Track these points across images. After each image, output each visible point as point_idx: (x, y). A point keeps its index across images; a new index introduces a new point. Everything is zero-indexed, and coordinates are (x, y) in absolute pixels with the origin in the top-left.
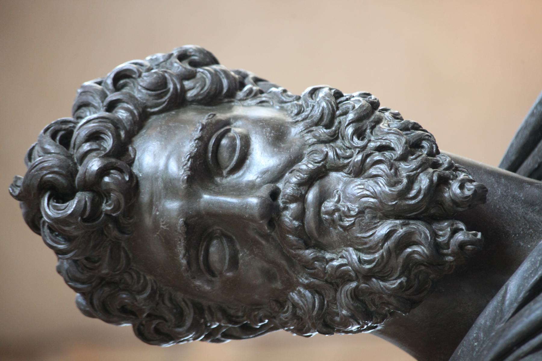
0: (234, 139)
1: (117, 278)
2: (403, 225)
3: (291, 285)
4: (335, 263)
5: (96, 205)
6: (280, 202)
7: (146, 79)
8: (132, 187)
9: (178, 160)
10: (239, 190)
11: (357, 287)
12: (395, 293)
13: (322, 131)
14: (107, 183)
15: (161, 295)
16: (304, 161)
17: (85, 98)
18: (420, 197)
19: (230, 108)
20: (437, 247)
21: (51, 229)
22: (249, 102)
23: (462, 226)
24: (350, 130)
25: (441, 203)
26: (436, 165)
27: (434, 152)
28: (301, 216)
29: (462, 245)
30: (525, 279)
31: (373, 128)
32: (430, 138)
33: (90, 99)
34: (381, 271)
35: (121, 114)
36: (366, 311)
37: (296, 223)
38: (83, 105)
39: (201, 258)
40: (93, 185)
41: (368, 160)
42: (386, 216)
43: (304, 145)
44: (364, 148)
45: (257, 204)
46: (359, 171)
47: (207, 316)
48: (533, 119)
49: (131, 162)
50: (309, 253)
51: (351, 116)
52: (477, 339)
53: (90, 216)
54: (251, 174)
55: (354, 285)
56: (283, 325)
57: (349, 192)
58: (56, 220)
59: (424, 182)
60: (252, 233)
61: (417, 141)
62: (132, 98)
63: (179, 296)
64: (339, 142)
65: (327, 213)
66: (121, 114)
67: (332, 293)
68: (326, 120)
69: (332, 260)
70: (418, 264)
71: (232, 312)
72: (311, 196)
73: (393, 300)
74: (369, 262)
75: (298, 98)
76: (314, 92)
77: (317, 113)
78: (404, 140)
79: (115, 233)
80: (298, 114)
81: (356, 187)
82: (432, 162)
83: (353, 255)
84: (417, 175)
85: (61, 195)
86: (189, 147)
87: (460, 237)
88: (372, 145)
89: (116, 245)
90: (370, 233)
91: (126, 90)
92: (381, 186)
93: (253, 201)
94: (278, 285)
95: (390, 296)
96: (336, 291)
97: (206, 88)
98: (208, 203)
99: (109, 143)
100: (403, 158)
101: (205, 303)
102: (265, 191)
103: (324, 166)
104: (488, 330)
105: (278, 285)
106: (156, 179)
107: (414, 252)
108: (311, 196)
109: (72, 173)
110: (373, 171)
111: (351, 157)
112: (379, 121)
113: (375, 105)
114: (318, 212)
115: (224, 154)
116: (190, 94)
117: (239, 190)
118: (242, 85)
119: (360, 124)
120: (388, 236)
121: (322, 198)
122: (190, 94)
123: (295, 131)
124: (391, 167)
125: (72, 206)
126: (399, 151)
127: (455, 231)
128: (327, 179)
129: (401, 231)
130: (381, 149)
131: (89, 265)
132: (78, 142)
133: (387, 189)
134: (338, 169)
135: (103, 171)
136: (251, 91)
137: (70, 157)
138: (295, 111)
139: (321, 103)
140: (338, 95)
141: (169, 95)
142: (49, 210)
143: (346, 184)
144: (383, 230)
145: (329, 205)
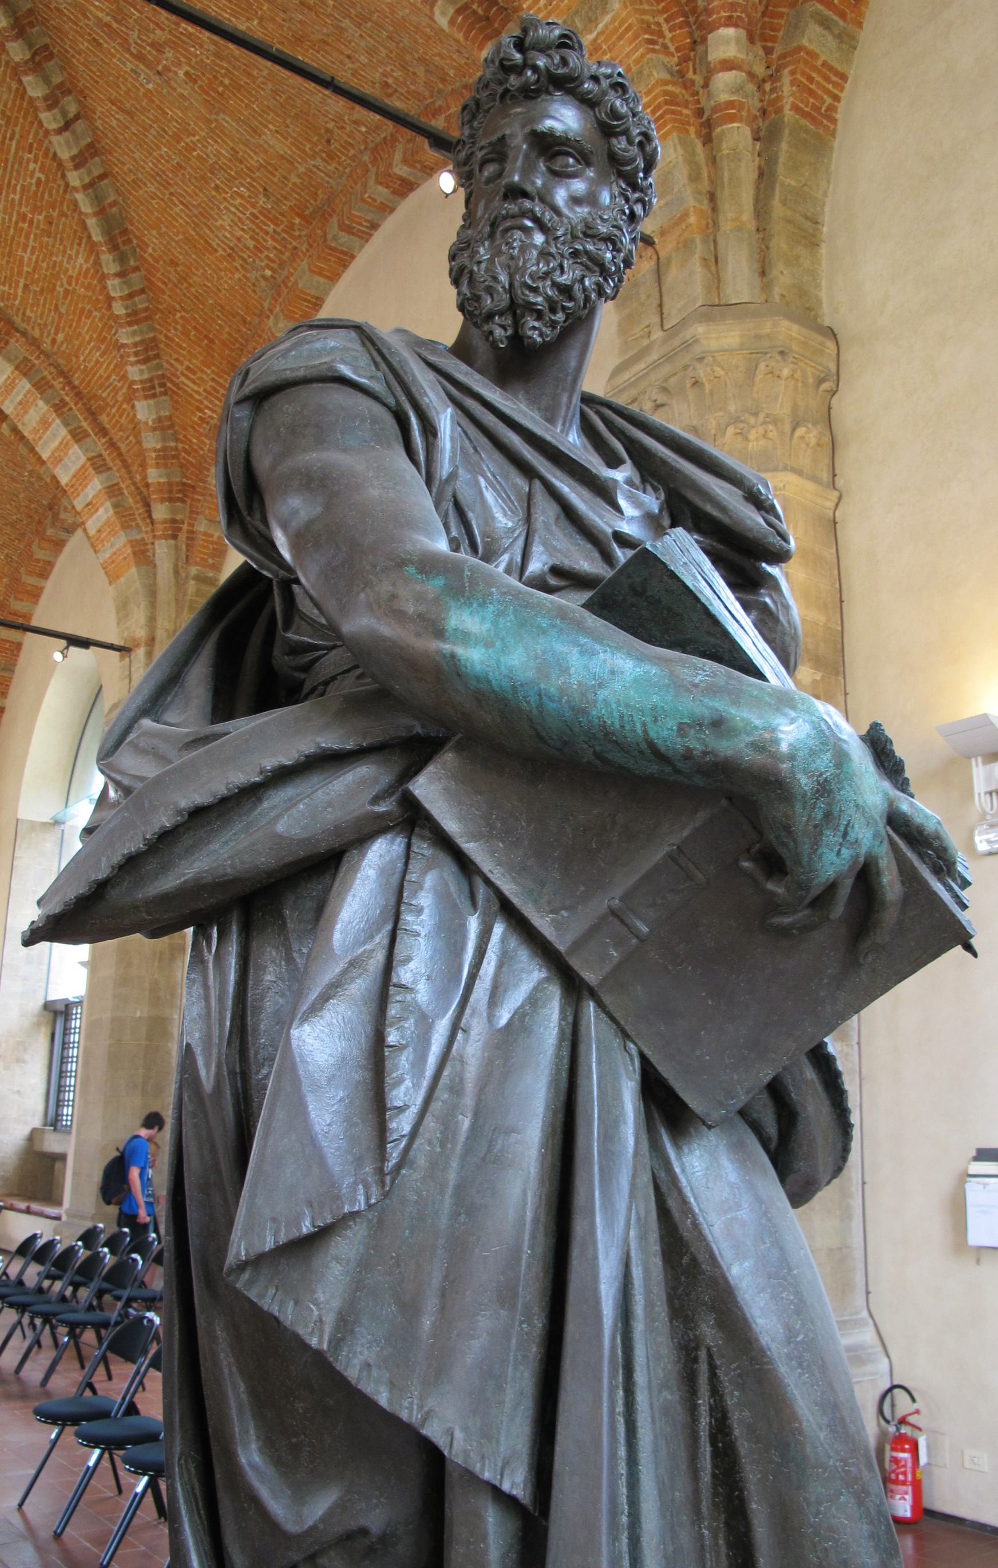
23: (510, 332)
68: (589, 232)
100: (555, 284)
127: (504, 327)
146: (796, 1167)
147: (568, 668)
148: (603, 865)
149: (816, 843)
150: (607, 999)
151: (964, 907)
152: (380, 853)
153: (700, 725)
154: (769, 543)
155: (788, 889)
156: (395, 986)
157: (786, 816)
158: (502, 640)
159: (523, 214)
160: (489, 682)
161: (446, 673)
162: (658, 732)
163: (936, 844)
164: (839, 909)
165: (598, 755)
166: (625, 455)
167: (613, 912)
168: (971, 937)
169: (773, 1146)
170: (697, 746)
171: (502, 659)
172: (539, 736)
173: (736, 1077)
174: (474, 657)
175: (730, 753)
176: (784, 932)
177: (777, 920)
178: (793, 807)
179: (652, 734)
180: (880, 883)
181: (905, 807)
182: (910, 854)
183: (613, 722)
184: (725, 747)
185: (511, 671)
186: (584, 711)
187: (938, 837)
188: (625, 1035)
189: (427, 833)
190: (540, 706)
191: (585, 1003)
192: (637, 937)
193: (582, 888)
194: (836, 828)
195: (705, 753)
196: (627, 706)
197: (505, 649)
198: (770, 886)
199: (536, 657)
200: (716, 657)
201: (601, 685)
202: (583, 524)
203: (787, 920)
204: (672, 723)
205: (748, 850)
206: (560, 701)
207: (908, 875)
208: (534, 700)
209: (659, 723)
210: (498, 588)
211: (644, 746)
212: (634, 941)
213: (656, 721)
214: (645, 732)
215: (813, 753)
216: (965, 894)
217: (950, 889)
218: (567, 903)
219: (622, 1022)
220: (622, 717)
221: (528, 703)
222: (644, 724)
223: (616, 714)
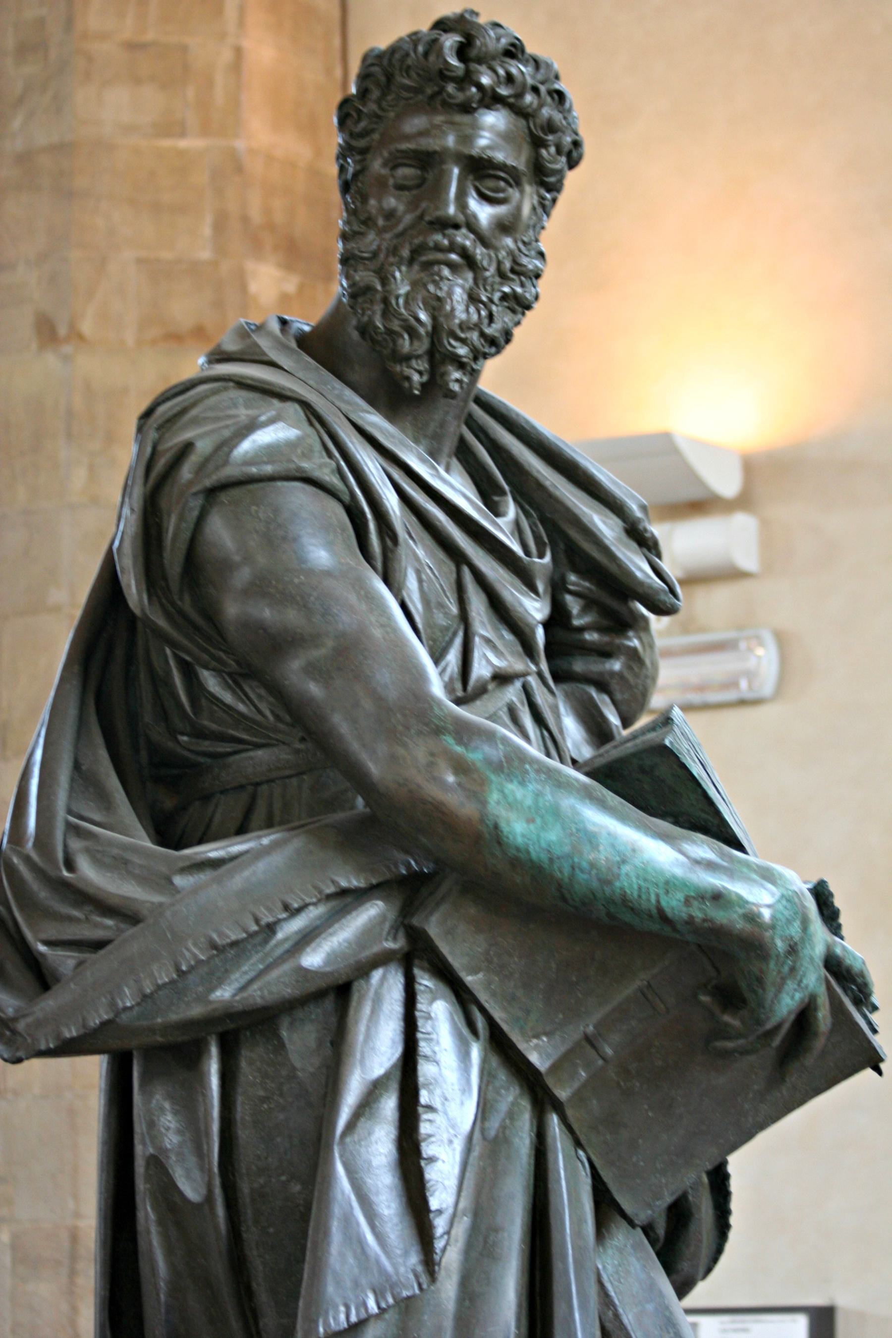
0: (503, 191)
1: (393, 88)
2: (427, 333)
3: (381, 231)
4: (398, 274)
5: (453, 79)
6: (450, 231)
7: (557, 117)
8: (467, 109)
9: (489, 147)
10: (461, 196)
11: (376, 290)
12: (371, 322)
13: (508, 265)
14: (470, 89)
15: (376, 123)
16: (484, 250)
17: (543, 66)
18: (449, 348)
19: (530, 184)
20: (407, 359)
21: (435, 41)
22: (536, 198)
23: (425, 378)
24: (506, 289)
25: (443, 363)
26: (475, 359)
27: (486, 356)
28: (438, 248)
29: (408, 379)
30: (380, 429)
31: (509, 308)
32: (498, 352)
33: (542, 71)
34: (388, 311)
35: (529, 98)
36: (358, 293)
37: (431, 244)
38: (537, 63)
39: (372, 526)
40: (468, 79)
41: (481, 306)
42: (434, 318)
43: (496, 249)
44: (491, 300)
45: (448, 214)
46: (473, 298)
47: (358, 157)
48: (514, 416)
49: (488, 107)
50: (406, 253)
51: (519, 290)
52: (334, 388)
53: (444, 74)
54: (474, 204)
55: (379, 288)
56: (347, 222)
57: (457, 291)
58: (441, 48)
59: (462, 351)
60: (424, 205)
61: (497, 344)
62: (541, 105)
63: (376, 136)
64: (497, 279)
65: (440, 270)
66: (529, 98)
67: (372, 267)
68: (517, 268)
69: (400, 271)
70: (394, 342)
71: (361, 178)
72: (454, 257)
73: (366, 319)
74: (397, 304)
75: (537, 241)
76: (541, 255)
77: (524, 261)
78: (497, 334)
79: (429, 91)
80: (524, 243)
81: (459, 294)
82: (478, 355)
83: (404, 289)
84: (467, 345)
85: (462, 52)
86: (500, 156)
87: (416, 377)
88: (494, 308)
89: (417, 91)
90: (421, 305)
91: (549, 99)
92: (461, 314)
93: (452, 210)
94: (381, 222)
95: (370, 317)
96: (374, 272)
97: (548, 165)
98: (451, 172)
99: (503, 91)
100: (482, 334)
101: (369, 156)
102: (461, 218)
103: (478, 267)
104: (340, 397)
105: (381, 222)
106: (473, 129)
107: (404, 339)
108: (454, 257)
109: (480, 61)
110: (472, 309)
111: (486, 290)
112: (514, 311)
113: (528, 307)
114: (439, 262)
115: (491, 183)
116: (544, 152)
117: (461, 196)
118: (549, 191)
119: (511, 298)
120: (418, 320)
121: (452, 266)
122: (544, 152)
123: (509, 242)
124: (476, 325)
125: (454, 61)
126: (488, 331)
127: (420, 373)
128: (466, 269)
129: (422, 331)
130: (491, 317)
131: (404, 67)
132: (507, 66)
133: (457, 321)
134: (475, 280)
135: (480, 87)
136: (543, 198)
137: (494, 58)
138: (525, 239)
139: (530, 263)
140: (538, 276)
141: (542, 135)
142: (450, 41)
143: (463, 287)
144: (423, 316)
145: (446, 272)
146: (679, 1267)
147: (598, 845)
148: (580, 995)
149: (780, 989)
150: (569, 1112)
151: (875, 1031)
152: (388, 986)
153: (703, 898)
154: (659, 601)
155: (743, 1022)
156: (423, 1106)
157: (761, 971)
158: (542, 817)
159: (452, 248)
160: (528, 852)
161: (487, 837)
162: (668, 902)
163: (859, 980)
164: (777, 1041)
165: (610, 915)
166: (507, 488)
167: (587, 1039)
168: (882, 1060)
169: (659, 1245)
170: (698, 915)
171: (542, 835)
172: (563, 899)
173: (663, 1181)
174: (517, 829)
175: (725, 921)
176: (725, 1054)
177: (719, 1044)
178: (768, 964)
179: (664, 903)
180: (816, 1017)
181: (838, 951)
182: (839, 990)
183: (632, 892)
184: (720, 916)
185: (549, 846)
186: (609, 883)
187: (862, 975)
188: (578, 1144)
189: (426, 965)
190: (572, 876)
191: (549, 1116)
192: (603, 1059)
193: (561, 1016)
194: (795, 978)
195: (704, 920)
196: (645, 880)
197: (544, 827)
198: (727, 1018)
199: (572, 834)
200: (705, 830)
201: (624, 862)
202: (511, 617)
203: (730, 1045)
204: (680, 896)
205: (705, 986)
206: (590, 873)
207: (837, 1008)
208: (567, 871)
209: (670, 895)
210: (530, 764)
211: (654, 911)
212: (600, 1062)
213: (667, 892)
214: (658, 901)
215: (789, 922)
216: (874, 1017)
217: (865, 1017)
218: (548, 1029)
219: (578, 1133)
220: (640, 888)
221: (561, 872)
222: (657, 895)
223: (635, 886)
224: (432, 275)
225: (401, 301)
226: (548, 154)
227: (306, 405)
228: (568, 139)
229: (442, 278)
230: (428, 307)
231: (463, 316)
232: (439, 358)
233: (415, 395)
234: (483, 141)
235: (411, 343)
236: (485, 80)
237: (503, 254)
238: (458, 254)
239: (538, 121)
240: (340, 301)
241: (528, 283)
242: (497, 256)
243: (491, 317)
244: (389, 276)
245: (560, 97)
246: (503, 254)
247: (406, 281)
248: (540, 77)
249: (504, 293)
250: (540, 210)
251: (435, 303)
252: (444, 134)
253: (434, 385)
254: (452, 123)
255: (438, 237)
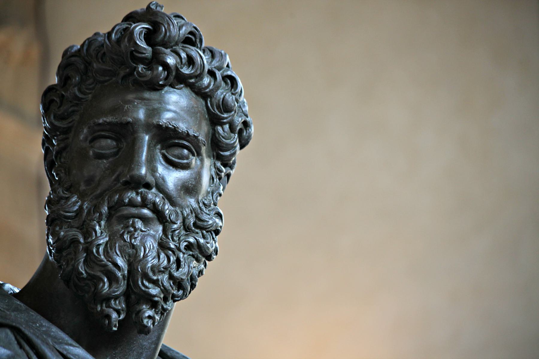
2: (124, 276)
3: (82, 196)
5: (142, 61)
7: (230, 98)
8: (155, 87)
9: (173, 119)
12: (75, 269)
13: (192, 220)
15: (77, 105)
16: (171, 207)
19: (209, 157)
20: (107, 299)
21: (126, 29)
24: (192, 240)
25: (138, 303)
26: (165, 300)
27: (175, 299)
28: (132, 204)
29: (109, 317)
31: (193, 256)
32: (184, 296)
33: (217, 59)
34: (91, 260)
35: (206, 80)
36: (63, 249)
37: (127, 201)
46: (163, 246)
49: (172, 86)
50: (105, 210)
51: (202, 241)
52: (41, 325)
53: (135, 55)
54: (161, 169)
55: (82, 240)
57: (148, 240)
58: (132, 33)
59: (154, 291)
60: (120, 169)
61: (183, 287)
62: (217, 88)
63: (76, 117)
64: (183, 232)
65: (134, 223)
66: (206, 80)
68: (200, 223)
74: (98, 252)
75: (215, 205)
76: (219, 215)
77: (205, 217)
79: (122, 73)
81: (151, 244)
83: (103, 241)
84: (159, 287)
85: (149, 37)
86: (182, 127)
87: (114, 315)
88: (181, 255)
91: (223, 83)
92: (151, 262)
94: (83, 187)
96: (78, 228)
98: (143, 139)
99: (186, 71)
100: (171, 277)
102: (150, 179)
103: (167, 221)
105: (83, 187)
106: (160, 103)
107: (104, 283)
110: (162, 255)
111: (173, 240)
113: (209, 258)
114: (134, 216)
115: (177, 151)
116: (219, 128)
118: (225, 166)
119: (196, 247)
121: (145, 220)
122: (219, 128)
123: (192, 201)
124: (165, 268)
125: (142, 44)
126: (176, 274)
127: (118, 312)
128: (158, 223)
129: (119, 274)
134: (165, 231)
135: (166, 66)
136: (221, 171)
137: (177, 44)
138: (206, 202)
139: (211, 220)
140: (217, 232)
142: (139, 28)
144: (120, 262)
145: (139, 224)
224: (128, 227)
225: (101, 249)
226: (222, 134)
227: (16, 331)
228: (239, 120)
229: (136, 230)
230: (123, 253)
231: (155, 261)
232: (135, 297)
233: (115, 331)
234: (167, 117)
235: (110, 286)
236: (171, 60)
237: (187, 211)
238: (148, 209)
239: (215, 102)
240: (46, 260)
241: (208, 235)
242: (183, 214)
243: (178, 262)
244: (90, 229)
245: (232, 81)
246: (187, 211)
247: (105, 234)
248: (215, 63)
249: (189, 242)
250: (216, 180)
251: (130, 251)
252: (137, 108)
253: (133, 325)
254: (143, 99)
255: (132, 195)
